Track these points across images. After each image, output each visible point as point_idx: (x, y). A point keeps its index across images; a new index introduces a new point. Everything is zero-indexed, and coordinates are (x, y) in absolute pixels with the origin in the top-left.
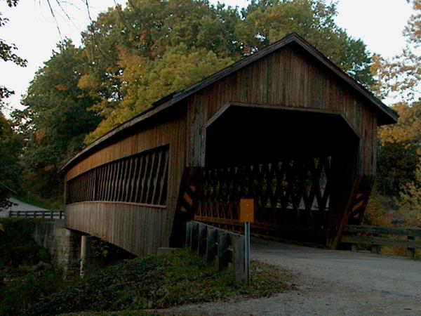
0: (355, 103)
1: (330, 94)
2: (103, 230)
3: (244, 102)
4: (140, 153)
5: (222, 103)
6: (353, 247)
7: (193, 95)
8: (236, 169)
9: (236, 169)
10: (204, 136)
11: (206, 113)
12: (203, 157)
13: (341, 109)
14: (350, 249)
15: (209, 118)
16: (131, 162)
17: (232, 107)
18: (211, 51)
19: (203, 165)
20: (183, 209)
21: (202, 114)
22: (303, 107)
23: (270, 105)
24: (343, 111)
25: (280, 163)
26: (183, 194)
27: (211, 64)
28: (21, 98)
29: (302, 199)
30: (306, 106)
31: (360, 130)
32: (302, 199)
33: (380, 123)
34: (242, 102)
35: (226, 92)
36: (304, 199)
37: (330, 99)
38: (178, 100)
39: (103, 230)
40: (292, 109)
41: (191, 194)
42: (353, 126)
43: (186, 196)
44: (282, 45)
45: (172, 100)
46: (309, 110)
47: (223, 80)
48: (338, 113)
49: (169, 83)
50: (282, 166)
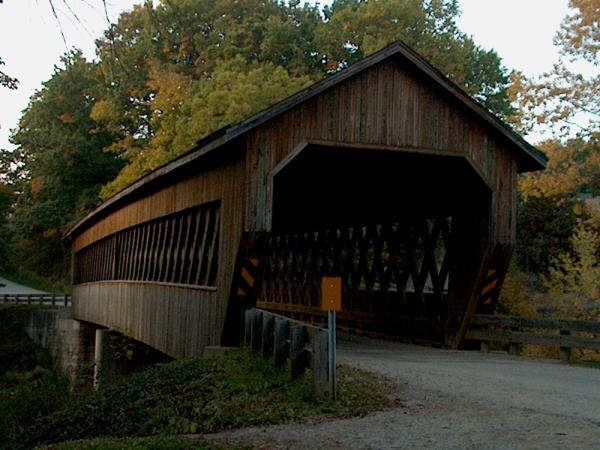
0: (486, 140)
8: (316, 234)
10: (270, 188)
12: (269, 216)
15: (278, 161)
19: (269, 228)
20: (241, 292)
22: (411, 146)
25: (379, 227)
30: (415, 145)
34: (325, 139)
38: (234, 136)
40: (396, 149)
41: (251, 269)
42: (483, 174)
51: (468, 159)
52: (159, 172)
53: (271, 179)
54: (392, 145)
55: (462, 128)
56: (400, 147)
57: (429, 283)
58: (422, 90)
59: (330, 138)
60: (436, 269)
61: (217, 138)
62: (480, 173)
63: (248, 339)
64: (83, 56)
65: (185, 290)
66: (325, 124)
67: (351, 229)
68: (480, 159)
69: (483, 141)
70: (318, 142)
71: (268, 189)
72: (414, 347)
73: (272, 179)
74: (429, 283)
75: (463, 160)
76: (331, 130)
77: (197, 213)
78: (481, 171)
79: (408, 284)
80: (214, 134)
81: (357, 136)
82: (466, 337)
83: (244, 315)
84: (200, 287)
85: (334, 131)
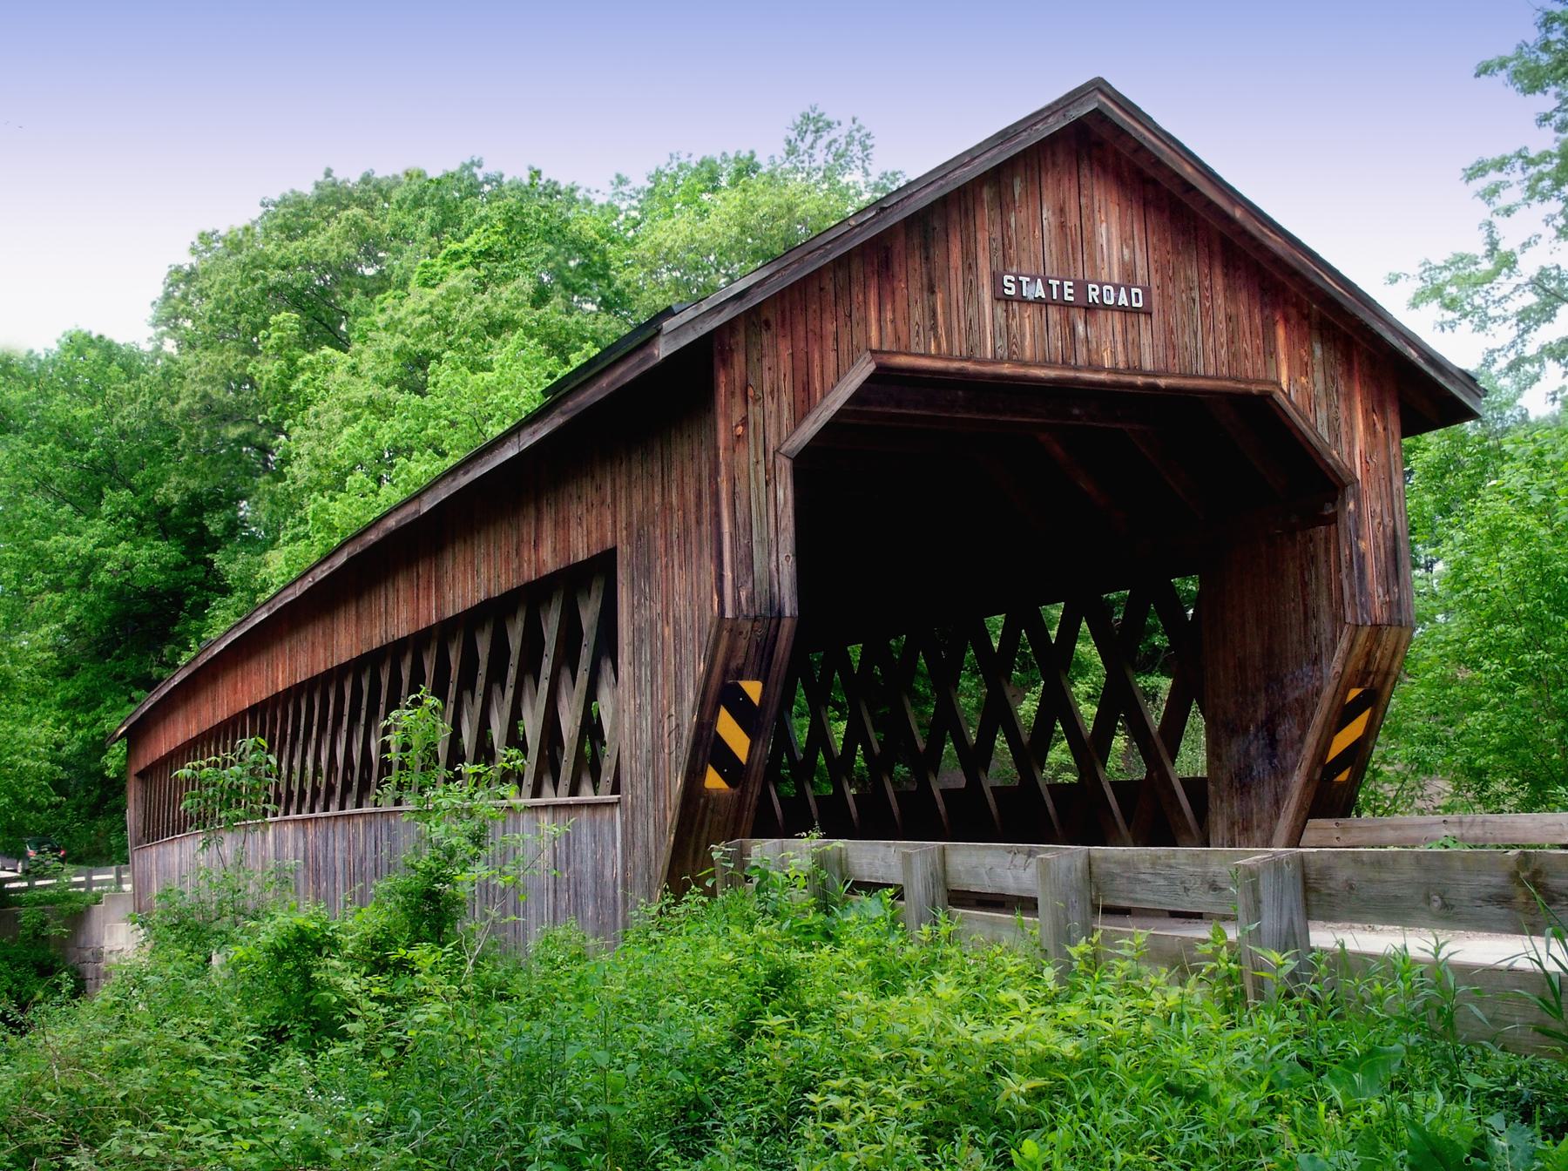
0: (1318, 352)
1: (1229, 318)
3: (927, 355)
5: (844, 357)
7: (730, 325)
10: (785, 492)
11: (786, 399)
12: (788, 569)
15: (799, 417)
16: (515, 642)
17: (884, 377)
18: (1480, 492)
20: (713, 780)
21: (771, 406)
22: (1140, 371)
26: (716, 714)
27: (1379, 612)
28: (321, 178)
30: (1148, 365)
31: (1345, 448)
33: (1413, 425)
35: (855, 315)
37: (1231, 341)
38: (684, 342)
40: (1103, 377)
41: (746, 715)
42: (1320, 438)
43: (729, 730)
45: (661, 340)
46: (1162, 382)
47: (843, 262)
49: (1061, 1033)
51: (1280, 398)
52: (391, 523)
55: (1258, 320)
57: (1059, 753)
58: (1153, 218)
59: (933, 350)
60: (866, 758)
62: (1314, 440)
68: (1312, 400)
70: (902, 361)
71: (780, 494)
74: (1059, 753)
75: (1266, 398)
77: (383, 663)
78: (1314, 428)
79: (1184, 748)
84: (342, 812)
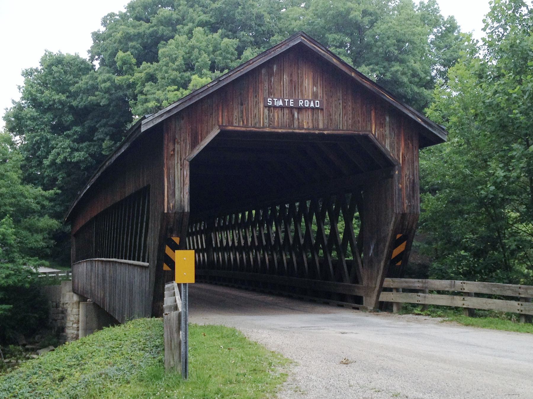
0: (387, 119)
2: (101, 295)
4: (130, 196)
6: (395, 308)
8: (254, 212)
9: (254, 212)
12: (187, 197)
13: (369, 129)
14: (391, 311)
15: (194, 145)
17: (223, 134)
19: (187, 209)
23: (333, 130)
24: (371, 131)
25: (297, 204)
29: (405, 242)
32: (405, 242)
34: (237, 126)
36: (407, 243)
38: (149, 127)
39: (101, 295)
40: (303, 131)
42: (387, 150)
44: (284, 49)
48: (367, 133)
50: (299, 206)
53: (187, 163)
54: (299, 128)
56: (306, 129)
61: (362, 75)
63: (425, 283)
64: (90, 49)
65: (100, 263)
66: (235, 114)
67: (297, 204)
69: (385, 119)
72: (309, 306)
73: (188, 163)
76: (242, 117)
80: (361, 74)
81: (266, 121)
82: (381, 299)
83: (401, 263)
85: (245, 118)
